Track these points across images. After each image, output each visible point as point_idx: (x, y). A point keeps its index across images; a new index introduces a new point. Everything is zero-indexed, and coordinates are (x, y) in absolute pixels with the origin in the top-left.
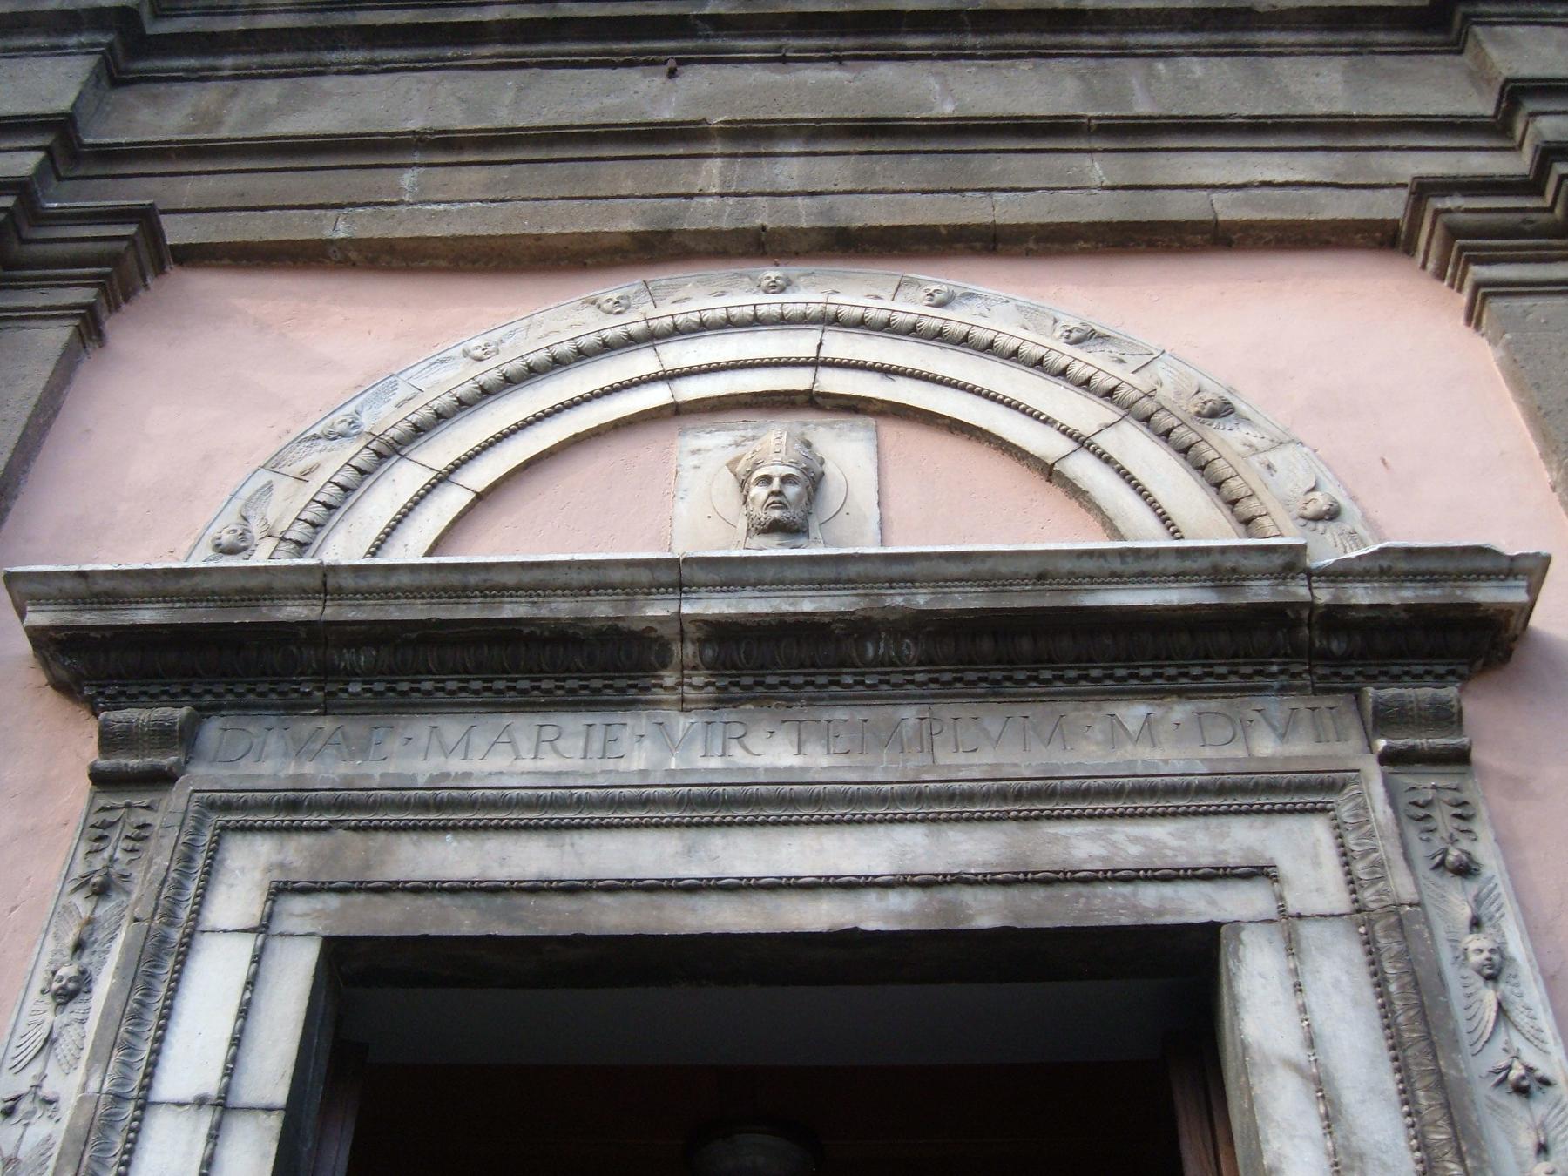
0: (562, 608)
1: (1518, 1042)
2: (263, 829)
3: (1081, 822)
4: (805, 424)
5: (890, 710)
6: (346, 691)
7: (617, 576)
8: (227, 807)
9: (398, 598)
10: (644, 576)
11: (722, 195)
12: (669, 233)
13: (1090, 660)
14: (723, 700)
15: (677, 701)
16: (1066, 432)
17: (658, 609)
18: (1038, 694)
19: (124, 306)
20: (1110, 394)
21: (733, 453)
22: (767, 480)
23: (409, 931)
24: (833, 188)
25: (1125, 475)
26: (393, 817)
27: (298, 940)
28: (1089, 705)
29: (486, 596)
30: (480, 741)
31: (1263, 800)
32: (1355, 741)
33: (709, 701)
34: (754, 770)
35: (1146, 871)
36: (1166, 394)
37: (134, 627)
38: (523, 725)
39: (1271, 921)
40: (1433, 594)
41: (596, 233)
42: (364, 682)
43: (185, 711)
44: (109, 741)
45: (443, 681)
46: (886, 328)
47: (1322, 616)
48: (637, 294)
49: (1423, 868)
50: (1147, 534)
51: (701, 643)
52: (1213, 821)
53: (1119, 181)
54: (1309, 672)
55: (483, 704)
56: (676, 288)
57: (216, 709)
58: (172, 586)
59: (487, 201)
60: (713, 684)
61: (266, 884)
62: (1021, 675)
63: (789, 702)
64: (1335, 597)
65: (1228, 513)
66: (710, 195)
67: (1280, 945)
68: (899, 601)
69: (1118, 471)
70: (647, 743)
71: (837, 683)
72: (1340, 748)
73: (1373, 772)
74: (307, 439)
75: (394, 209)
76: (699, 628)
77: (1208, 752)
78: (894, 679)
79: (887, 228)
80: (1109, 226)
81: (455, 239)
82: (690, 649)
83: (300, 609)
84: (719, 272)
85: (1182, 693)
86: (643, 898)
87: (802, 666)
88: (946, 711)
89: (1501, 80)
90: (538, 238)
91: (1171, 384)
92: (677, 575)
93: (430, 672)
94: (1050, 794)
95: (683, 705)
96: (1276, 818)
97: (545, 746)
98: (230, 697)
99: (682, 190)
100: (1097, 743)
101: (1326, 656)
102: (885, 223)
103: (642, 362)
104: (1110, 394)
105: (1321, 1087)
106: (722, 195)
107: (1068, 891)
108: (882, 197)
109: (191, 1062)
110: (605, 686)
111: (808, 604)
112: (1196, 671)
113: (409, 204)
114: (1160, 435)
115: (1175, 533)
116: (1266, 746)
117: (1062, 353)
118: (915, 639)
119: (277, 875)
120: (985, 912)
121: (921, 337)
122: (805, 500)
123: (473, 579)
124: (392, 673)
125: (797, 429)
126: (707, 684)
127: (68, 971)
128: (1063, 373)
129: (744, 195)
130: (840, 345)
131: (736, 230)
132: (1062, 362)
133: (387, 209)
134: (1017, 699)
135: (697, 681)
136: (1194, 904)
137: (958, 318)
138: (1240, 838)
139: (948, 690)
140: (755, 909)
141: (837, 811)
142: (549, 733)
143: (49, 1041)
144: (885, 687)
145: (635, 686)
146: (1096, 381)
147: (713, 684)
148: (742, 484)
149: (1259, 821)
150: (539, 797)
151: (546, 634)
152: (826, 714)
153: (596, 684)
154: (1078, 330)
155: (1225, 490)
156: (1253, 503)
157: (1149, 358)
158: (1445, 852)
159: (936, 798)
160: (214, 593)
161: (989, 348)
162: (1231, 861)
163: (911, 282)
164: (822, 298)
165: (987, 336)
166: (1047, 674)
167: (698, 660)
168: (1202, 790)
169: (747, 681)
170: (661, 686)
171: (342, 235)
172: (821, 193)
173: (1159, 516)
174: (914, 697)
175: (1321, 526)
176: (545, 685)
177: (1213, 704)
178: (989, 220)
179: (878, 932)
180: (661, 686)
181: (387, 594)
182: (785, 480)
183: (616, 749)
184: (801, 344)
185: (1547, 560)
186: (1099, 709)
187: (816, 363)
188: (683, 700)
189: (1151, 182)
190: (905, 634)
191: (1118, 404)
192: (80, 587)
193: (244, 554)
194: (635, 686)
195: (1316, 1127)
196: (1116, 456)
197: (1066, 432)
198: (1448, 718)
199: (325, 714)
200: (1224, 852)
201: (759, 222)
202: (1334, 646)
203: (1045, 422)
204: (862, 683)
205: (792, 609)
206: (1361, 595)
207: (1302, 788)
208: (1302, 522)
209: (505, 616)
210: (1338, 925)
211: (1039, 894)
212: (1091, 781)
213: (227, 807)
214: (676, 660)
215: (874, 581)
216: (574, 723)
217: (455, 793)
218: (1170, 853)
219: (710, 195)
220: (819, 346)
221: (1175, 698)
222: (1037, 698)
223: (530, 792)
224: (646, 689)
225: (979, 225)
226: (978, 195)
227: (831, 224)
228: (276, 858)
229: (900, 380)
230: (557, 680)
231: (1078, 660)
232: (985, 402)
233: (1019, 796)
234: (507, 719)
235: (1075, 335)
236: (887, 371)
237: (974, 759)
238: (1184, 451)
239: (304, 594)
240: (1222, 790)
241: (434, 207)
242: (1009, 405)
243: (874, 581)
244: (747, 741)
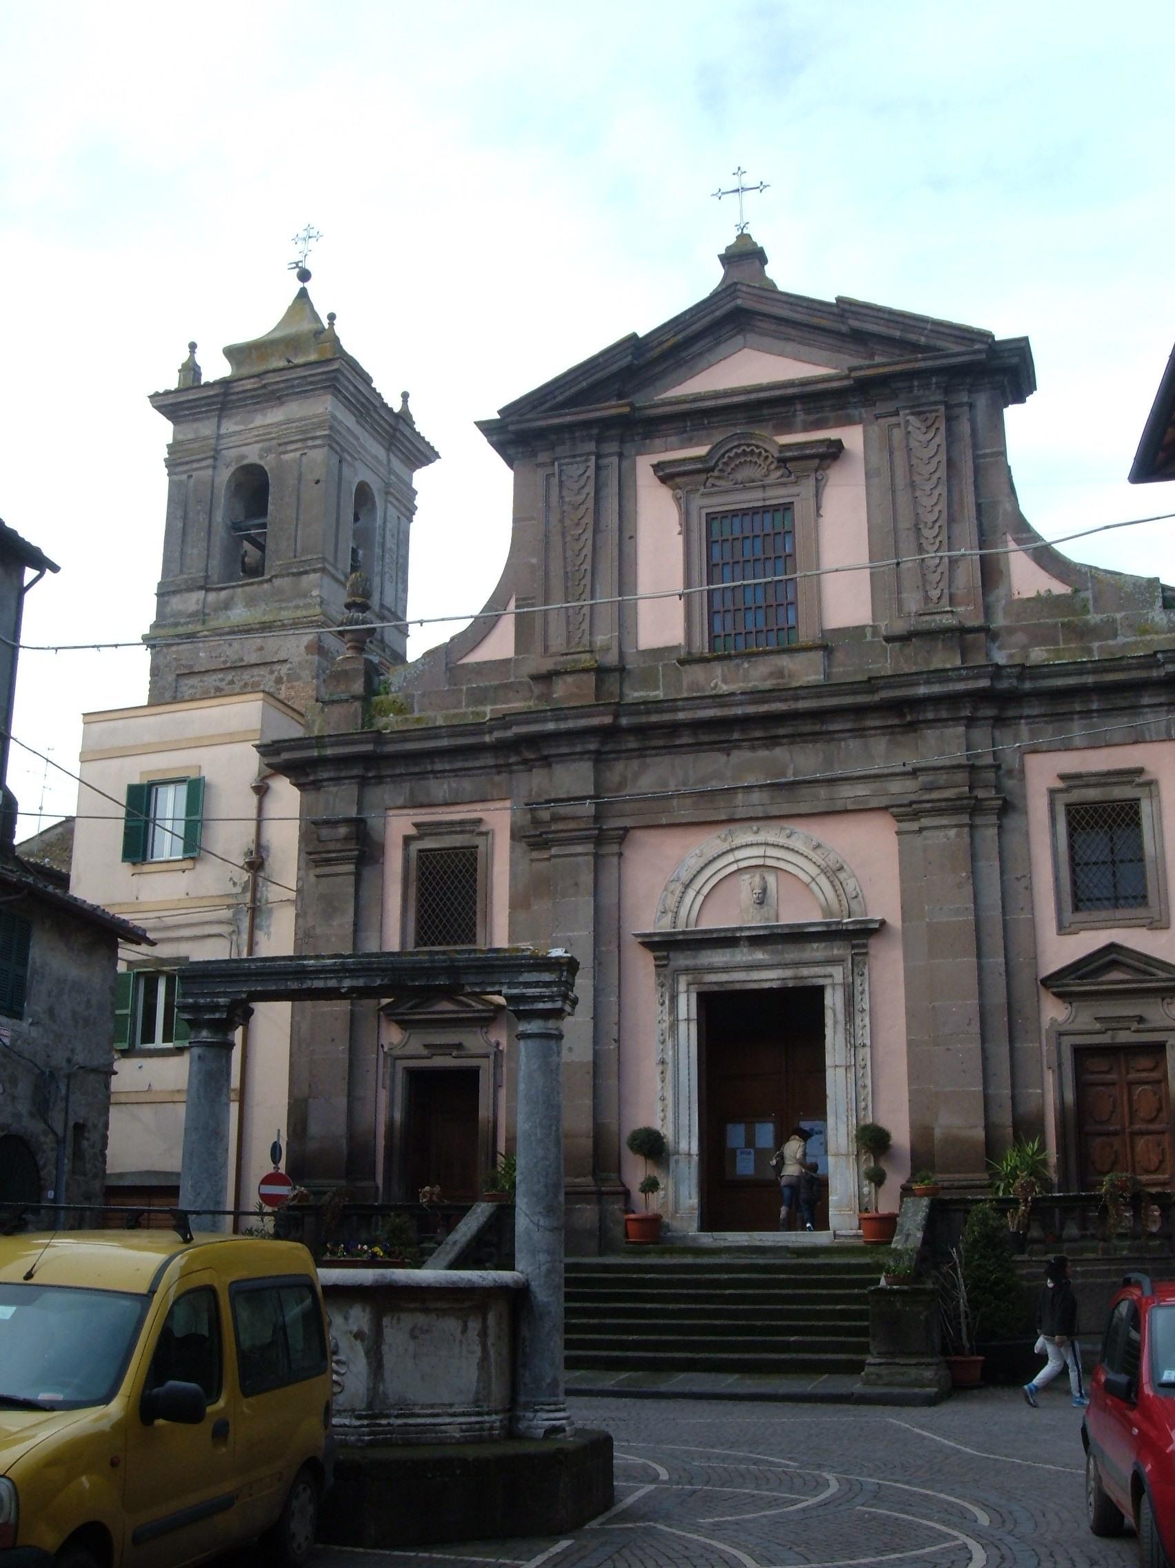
5: (877, 784)
40: (863, 926)
44: (656, 959)
103: (730, 858)
109: (682, 1014)
111: (762, 933)
117: (811, 854)
130: (771, 852)
136: (821, 982)
138: (829, 970)
198: (865, 946)
236: (778, 859)
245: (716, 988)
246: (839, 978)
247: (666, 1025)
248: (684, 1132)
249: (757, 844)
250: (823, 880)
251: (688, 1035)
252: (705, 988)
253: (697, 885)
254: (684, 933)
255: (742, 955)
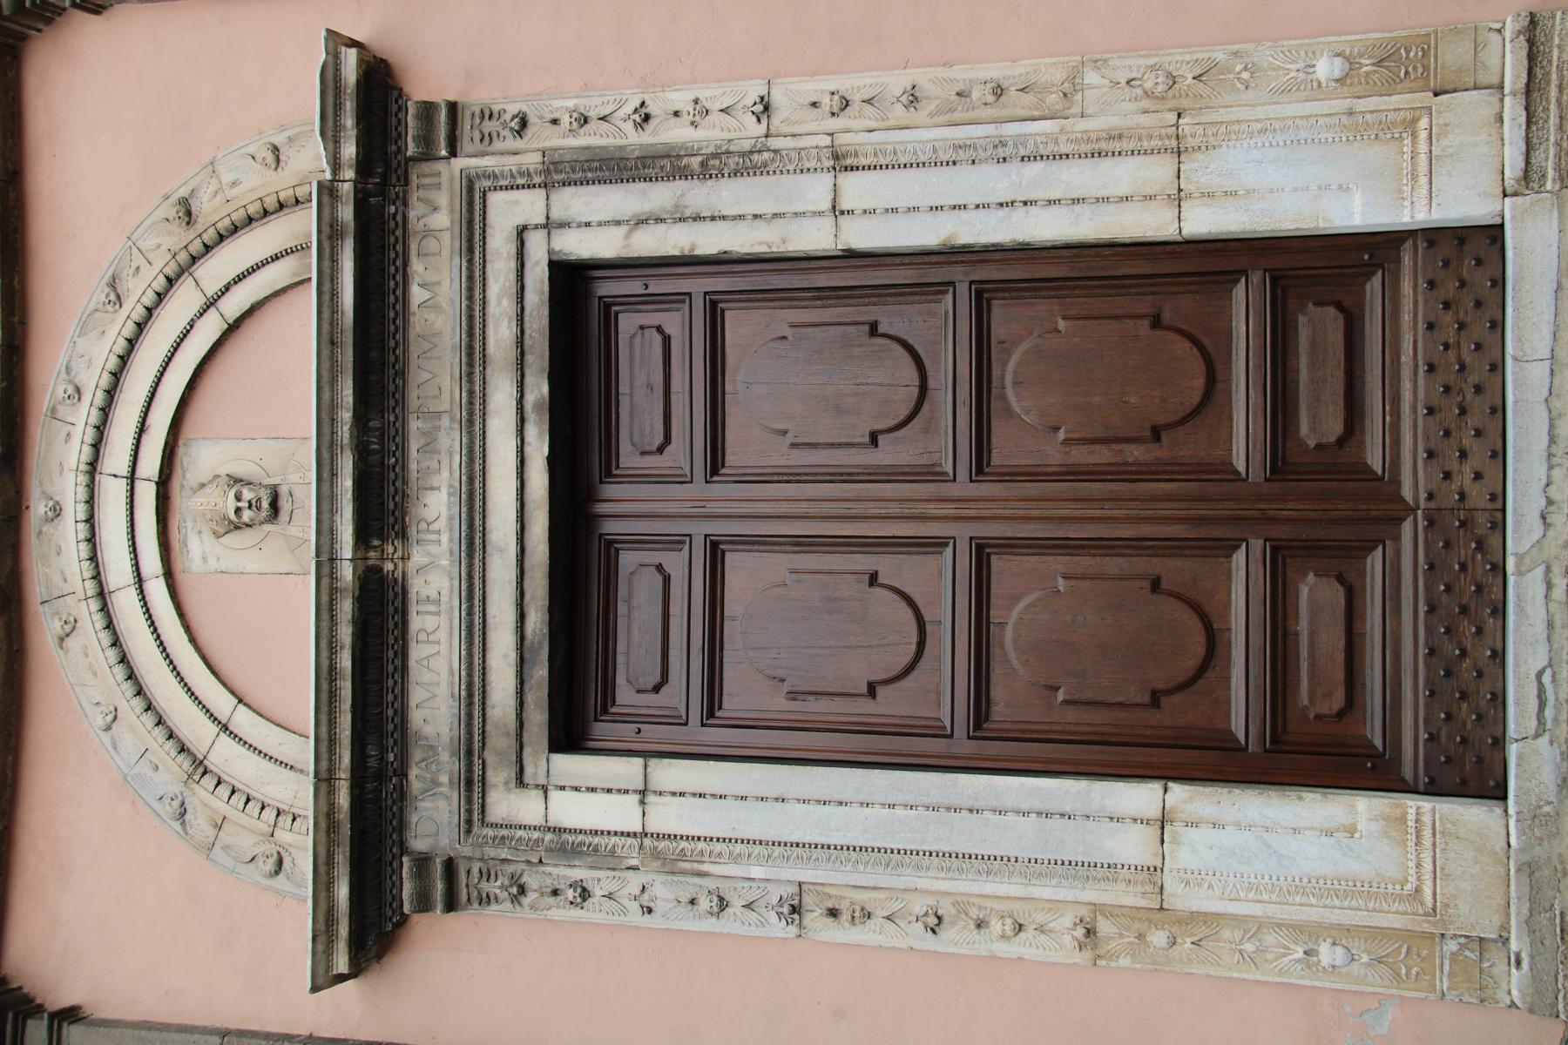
1: (621, 114)
4: (182, 486)
7: (325, 598)
8: (469, 822)
10: (325, 582)
14: (403, 535)
17: (347, 572)
19: (38, 1001)
20: (170, 281)
22: (238, 510)
25: (239, 279)
30: (427, 677)
32: (441, 166)
34: (451, 518)
37: (351, 898)
40: (349, 106)
44: (423, 903)
49: (519, 144)
52: (488, 257)
58: (323, 878)
62: (392, 358)
63: (405, 496)
67: (559, 231)
68: (346, 428)
73: (459, 163)
77: (446, 253)
82: (372, 554)
85: (406, 264)
86: (527, 575)
88: (413, 402)
89: (1533, 676)
91: (164, 244)
94: (470, 347)
95: (405, 558)
101: (385, 177)
103: (126, 604)
104: (170, 281)
105: (641, 221)
107: (528, 342)
109: (619, 814)
111: (347, 483)
112: (393, 255)
117: (133, 309)
118: (369, 420)
120: (538, 388)
125: (187, 492)
127: (570, 894)
128: (150, 311)
130: (116, 457)
135: (391, 549)
136: (538, 276)
137: (94, 380)
138: (500, 243)
139: (401, 402)
141: (477, 467)
142: (422, 637)
143: (610, 896)
146: (159, 289)
148: (237, 528)
149: (489, 231)
152: (414, 475)
157: (135, 250)
158: (512, 129)
162: (514, 250)
168: (470, 261)
175: (282, 158)
177: (413, 247)
182: (238, 498)
184: (113, 493)
185: (328, 30)
190: (366, 425)
192: (322, 939)
195: (662, 226)
198: (428, 109)
206: (349, 150)
207: (471, 204)
210: (553, 197)
211: (529, 358)
213: (469, 822)
216: (416, 623)
222: (406, 350)
224: (396, 580)
228: (502, 788)
233: (471, 365)
234: (412, 663)
236: (142, 429)
238: (221, 238)
239: (332, 792)
240: (471, 250)
243: (332, 444)
245: (540, 673)
246: (526, 206)
247: (663, 890)
248: (1070, 842)
249: (90, 501)
250: (215, 270)
251: (701, 798)
252: (538, 717)
253: (197, 730)
254: (324, 780)
255: (430, 569)
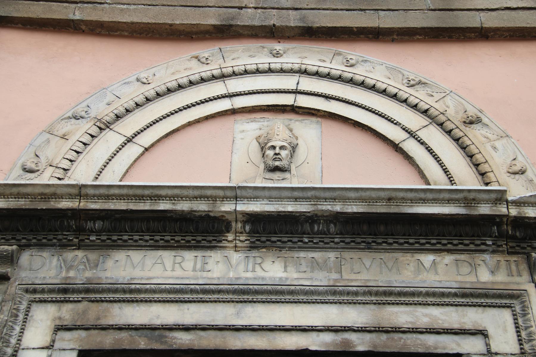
0: (184, 206)
2: (52, 302)
3: (402, 306)
4: (291, 120)
5: (324, 253)
6: (89, 239)
7: (209, 193)
8: (35, 291)
9: (113, 199)
10: (221, 193)
11: (255, 8)
12: (231, 26)
13: (409, 235)
14: (252, 247)
15: (232, 247)
16: (404, 129)
17: (227, 207)
18: (386, 249)
20: (425, 112)
21: (258, 133)
22: (274, 147)
23: (117, 347)
24: (306, 7)
26: (111, 296)
27: (67, 352)
28: (408, 255)
29: (152, 200)
30: (149, 262)
31: (482, 301)
33: (247, 247)
35: (430, 329)
36: (451, 113)
38: (167, 256)
39: (484, 355)
41: (198, 24)
42: (97, 235)
43: (15, 247)
45: (132, 236)
46: (328, 76)
47: (512, 221)
48: (213, 55)
50: (439, 182)
51: (244, 223)
52: (460, 308)
53: (437, 7)
54: (506, 245)
55: (149, 246)
56: (234, 51)
57: (28, 246)
58: (8, 191)
59: (147, 5)
60: (248, 240)
61: (53, 326)
62: (380, 241)
63: (281, 248)
64: (519, 213)
65: (474, 169)
66: (250, 8)
68: (329, 207)
69: (427, 148)
70: (220, 265)
71: (301, 241)
72: (517, 279)
74: (65, 119)
75: (102, 6)
76: (243, 216)
77: (459, 278)
78: (326, 240)
79: (329, 27)
80: (431, 29)
81: (132, 23)
82: (239, 225)
83: (69, 203)
84: (253, 45)
85: (449, 251)
87: (287, 233)
88: (348, 255)
90: (171, 25)
91: (452, 110)
92: (235, 193)
93: (126, 232)
96: (488, 309)
97: (177, 266)
98: (34, 241)
99: (237, 5)
100: (411, 272)
101: (513, 238)
102: (329, 25)
103: (217, 88)
106: (255, 8)
107: (396, 336)
108: (328, 12)
110: (203, 240)
111: (290, 207)
112: (455, 242)
113: (110, 4)
114: (446, 132)
115: (451, 181)
116: (484, 276)
117: (405, 92)
118: (335, 225)
119: (58, 323)
121: (343, 81)
122: (290, 156)
123: (147, 192)
124: (109, 231)
125: (287, 122)
126: (246, 240)
129: (265, 8)
130: (308, 84)
131: (262, 26)
132: (405, 96)
133: (99, 5)
134: (377, 250)
135: (242, 238)
137: (360, 72)
138: (471, 317)
139: (347, 247)
140: (264, 339)
142: (179, 259)
144: (322, 244)
145: (215, 240)
147: (248, 240)
148: (262, 148)
149: (480, 309)
150: (174, 288)
151: (178, 217)
152: (296, 254)
153: (199, 238)
154: (413, 80)
155: (474, 159)
156: (486, 165)
159: (341, 293)
160: (28, 195)
161: (373, 88)
162: (467, 327)
163: (339, 54)
164: (299, 61)
165: (372, 82)
166: (391, 241)
167: (243, 230)
168: (455, 295)
169: (264, 239)
170: (227, 240)
171: (78, 18)
172: (301, 9)
173: (444, 170)
174: (334, 248)
176: (177, 238)
177: (462, 257)
178: (376, 25)
179: (316, 351)
180: (227, 240)
181: (108, 197)
183: (208, 267)
184: (289, 82)
186: (413, 257)
187: (296, 92)
188: (236, 247)
189: (453, 8)
190: (331, 222)
191: (428, 117)
193: (36, 174)
194: (215, 240)
196: (426, 142)
197: (404, 129)
199: (79, 249)
200: (464, 323)
201: (272, 23)
202: (518, 234)
203: (396, 124)
204: (312, 241)
205: (283, 210)
208: (509, 174)
209: (160, 209)
211: (384, 337)
212: (408, 289)
214: (233, 229)
215: (318, 198)
217: (138, 286)
218: (440, 322)
219: (250, 8)
220: (298, 83)
221: (446, 253)
223: (171, 286)
225: (371, 28)
226: (372, 12)
227: (305, 25)
228: (57, 315)
229: (333, 102)
230: (182, 236)
231: (404, 235)
232: (370, 113)
233: (377, 294)
234: (160, 253)
235: (412, 82)
236: (328, 97)
237: (359, 277)
238: (457, 140)
239: (71, 196)
240: (464, 295)
241: (122, 6)
242: (380, 115)
243: (318, 198)
244: (263, 265)
245: (142, 343)
